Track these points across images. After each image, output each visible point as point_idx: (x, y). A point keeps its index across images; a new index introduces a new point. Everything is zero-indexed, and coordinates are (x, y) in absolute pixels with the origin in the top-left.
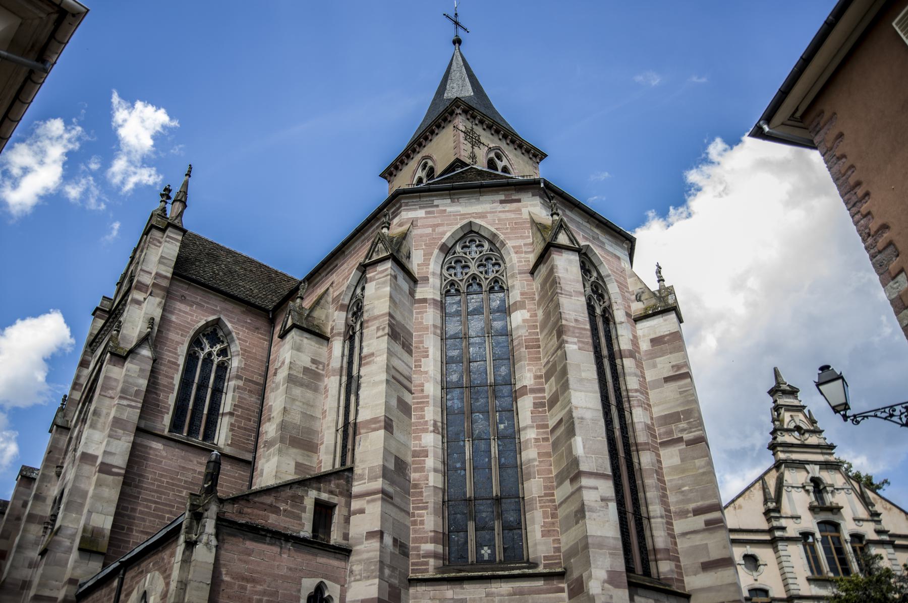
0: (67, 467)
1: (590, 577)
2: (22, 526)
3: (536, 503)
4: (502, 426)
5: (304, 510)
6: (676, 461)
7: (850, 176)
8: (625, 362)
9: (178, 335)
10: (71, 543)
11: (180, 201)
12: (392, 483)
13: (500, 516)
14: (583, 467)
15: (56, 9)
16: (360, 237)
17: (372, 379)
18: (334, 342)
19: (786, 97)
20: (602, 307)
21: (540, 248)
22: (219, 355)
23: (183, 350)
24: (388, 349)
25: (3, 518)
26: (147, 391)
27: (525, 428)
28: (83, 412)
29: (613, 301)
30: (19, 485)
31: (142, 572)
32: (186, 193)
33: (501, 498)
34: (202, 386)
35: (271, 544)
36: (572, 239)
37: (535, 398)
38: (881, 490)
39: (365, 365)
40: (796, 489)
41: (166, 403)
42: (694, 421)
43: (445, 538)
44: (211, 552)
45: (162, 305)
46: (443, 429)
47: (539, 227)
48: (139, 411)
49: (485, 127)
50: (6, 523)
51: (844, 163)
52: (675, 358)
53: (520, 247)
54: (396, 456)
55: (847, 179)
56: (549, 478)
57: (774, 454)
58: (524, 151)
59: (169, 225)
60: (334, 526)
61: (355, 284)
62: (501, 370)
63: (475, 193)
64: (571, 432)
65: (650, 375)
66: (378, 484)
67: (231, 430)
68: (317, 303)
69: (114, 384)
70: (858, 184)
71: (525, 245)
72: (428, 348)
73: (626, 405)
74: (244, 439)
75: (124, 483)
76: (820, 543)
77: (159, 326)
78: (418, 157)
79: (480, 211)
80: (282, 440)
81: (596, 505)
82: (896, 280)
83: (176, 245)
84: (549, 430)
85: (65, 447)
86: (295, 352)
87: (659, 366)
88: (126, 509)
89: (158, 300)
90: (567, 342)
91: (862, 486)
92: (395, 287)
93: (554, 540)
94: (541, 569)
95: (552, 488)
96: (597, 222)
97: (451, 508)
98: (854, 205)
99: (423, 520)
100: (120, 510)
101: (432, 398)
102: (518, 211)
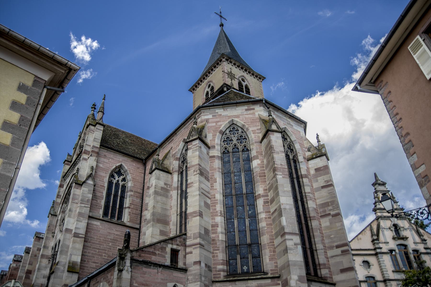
0: (57, 233)
1: (291, 278)
2: (39, 260)
3: (266, 246)
4: (250, 212)
5: (166, 253)
6: (328, 224)
7: (394, 110)
8: (304, 180)
9: (104, 173)
10: (64, 268)
11: (101, 111)
12: (204, 239)
13: (251, 252)
14: (286, 230)
15: (68, 68)
16: (183, 127)
17: (193, 194)
18: (174, 175)
19: (367, 75)
20: (293, 155)
21: (264, 131)
22: (122, 181)
23: (106, 180)
24: (199, 180)
25: (29, 255)
26: (92, 199)
27: (260, 213)
28: (63, 208)
29: (298, 152)
30: (35, 241)
31: (98, 282)
32: (103, 108)
33: (251, 244)
34: (116, 196)
35: (154, 269)
36: (278, 127)
37: (264, 199)
38: (429, 227)
39: (189, 187)
40: (386, 229)
41: (100, 204)
42: (335, 206)
43: (228, 263)
44: (129, 274)
45: (96, 160)
46: (224, 214)
47: (264, 122)
48: (89, 209)
49: (236, 67)
50: (30, 258)
51: (391, 104)
52: (326, 177)
53: (255, 130)
54: (204, 228)
55: (393, 111)
56: (272, 235)
57: (375, 214)
58: (255, 77)
59: (97, 123)
60: (179, 260)
61: (182, 148)
62: (249, 187)
63: (234, 106)
64: (280, 215)
65: (315, 185)
66: (198, 240)
67: (129, 215)
68: (165, 157)
69: (77, 197)
70: (397, 114)
71: (257, 129)
72: (216, 178)
73: (305, 200)
74: (135, 218)
75: (85, 241)
76: (398, 255)
77: (96, 170)
78: (206, 81)
79: (236, 114)
80: (153, 220)
81: (292, 247)
82: (412, 157)
83: (101, 132)
84: (271, 213)
85: (55, 224)
86: (157, 180)
87: (319, 181)
88: (85, 252)
89: (94, 158)
90: (277, 175)
91: (417, 227)
92: (201, 152)
93: (275, 263)
94: (269, 275)
95: (273, 239)
96: (289, 116)
97: (229, 249)
98: (396, 123)
99: (218, 255)
100: (83, 253)
101: (219, 201)
102: (254, 114)
